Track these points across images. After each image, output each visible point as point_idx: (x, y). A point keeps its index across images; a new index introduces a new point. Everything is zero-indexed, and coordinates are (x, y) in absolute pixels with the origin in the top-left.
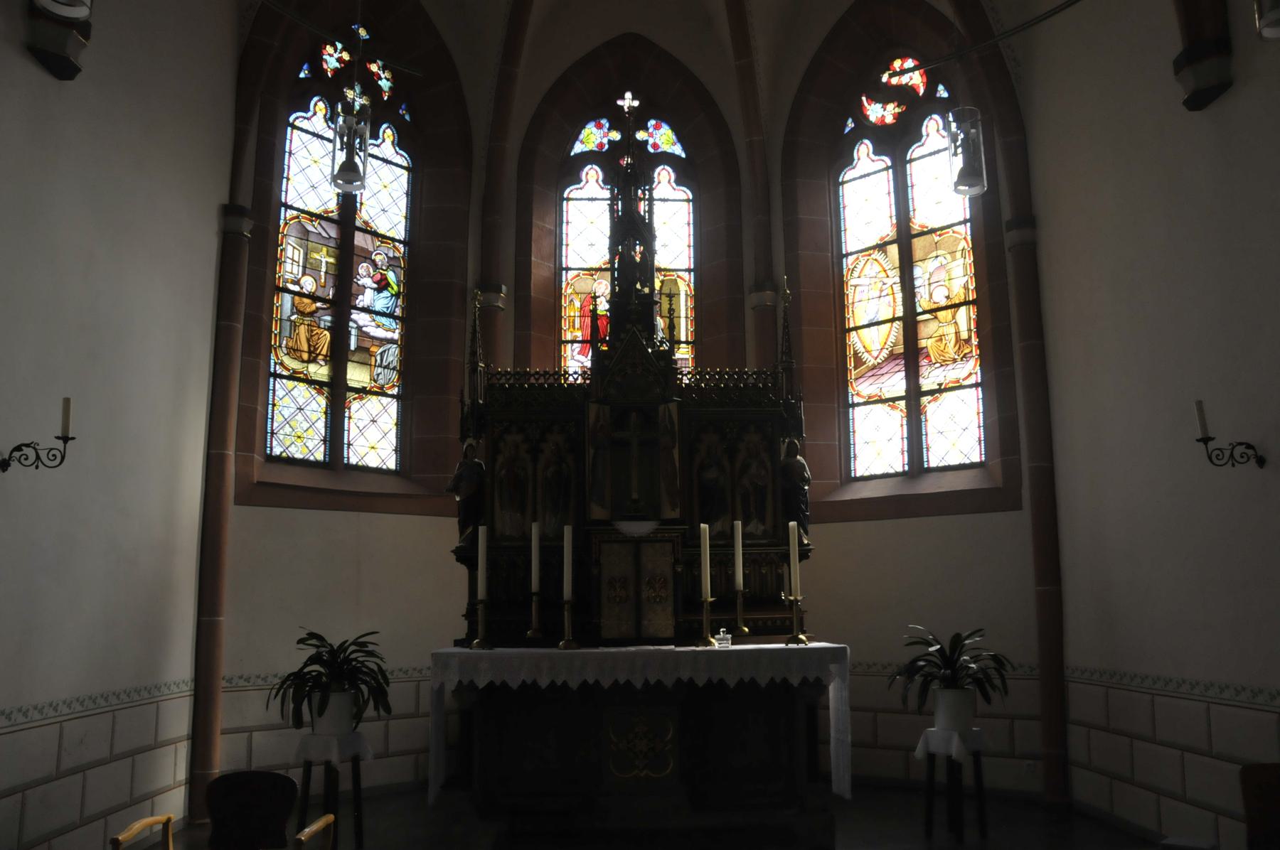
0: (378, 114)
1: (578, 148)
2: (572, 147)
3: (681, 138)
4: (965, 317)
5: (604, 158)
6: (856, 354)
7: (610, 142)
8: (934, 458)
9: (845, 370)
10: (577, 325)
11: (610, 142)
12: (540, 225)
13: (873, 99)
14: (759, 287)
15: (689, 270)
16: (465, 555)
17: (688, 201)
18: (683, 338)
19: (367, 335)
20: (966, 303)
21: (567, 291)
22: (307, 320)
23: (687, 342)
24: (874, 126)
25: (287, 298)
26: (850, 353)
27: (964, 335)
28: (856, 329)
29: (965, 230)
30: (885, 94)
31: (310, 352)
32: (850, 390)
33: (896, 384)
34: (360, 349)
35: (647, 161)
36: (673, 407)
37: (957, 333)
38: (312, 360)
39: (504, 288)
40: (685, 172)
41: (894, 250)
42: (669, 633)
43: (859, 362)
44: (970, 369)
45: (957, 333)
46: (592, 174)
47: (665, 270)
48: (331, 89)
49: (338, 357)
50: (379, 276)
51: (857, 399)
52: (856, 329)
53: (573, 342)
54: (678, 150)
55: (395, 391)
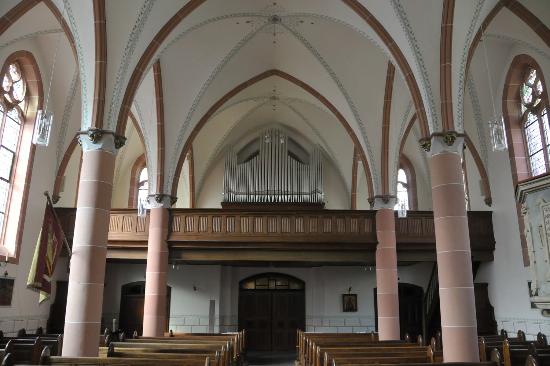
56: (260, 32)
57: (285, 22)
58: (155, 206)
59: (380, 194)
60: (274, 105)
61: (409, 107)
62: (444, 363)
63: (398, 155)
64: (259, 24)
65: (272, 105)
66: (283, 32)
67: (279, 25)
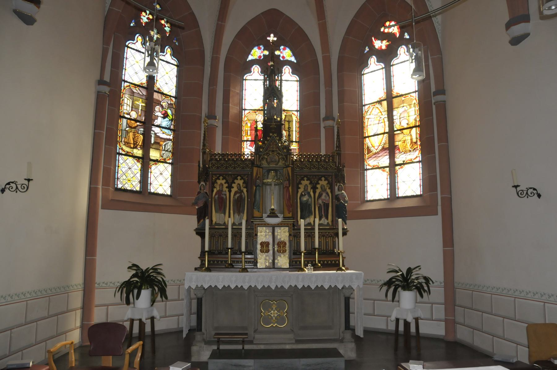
1: (250, 58)
4: (415, 133)
6: (368, 147)
7: (264, 55)
8: (401, 193)
9: (363, 154)
10: (249, 134)
11: (264, 55)
12: (234, 90)
13: (377, 39)
15: (297, 111)
17: (297, 81)
18: (294, 140)
19: (159, 137)
20: (415, 126)
22: (133, 130)
23: (296, 142)
26: (365, 147)
28: (368, 137)
29: (416, 95)
31: (134, 144)
32: (365, 163)
33: (385, 161)
34: (155, 143)
37: (411, 139)
38: (135, 147)
40: (296, 69)
41: (385, 103)
42: (287, 266)
43: (369, 151)
44: (416, 155)
45: (411, 139)
46: (256, 69)
47: (287, 111)
48: (144, 31)
50: (164, 112)
51: (368, 167)
52: (368, 137)
53: (247, 141)
54: (293, 59)
55: (170, 161)
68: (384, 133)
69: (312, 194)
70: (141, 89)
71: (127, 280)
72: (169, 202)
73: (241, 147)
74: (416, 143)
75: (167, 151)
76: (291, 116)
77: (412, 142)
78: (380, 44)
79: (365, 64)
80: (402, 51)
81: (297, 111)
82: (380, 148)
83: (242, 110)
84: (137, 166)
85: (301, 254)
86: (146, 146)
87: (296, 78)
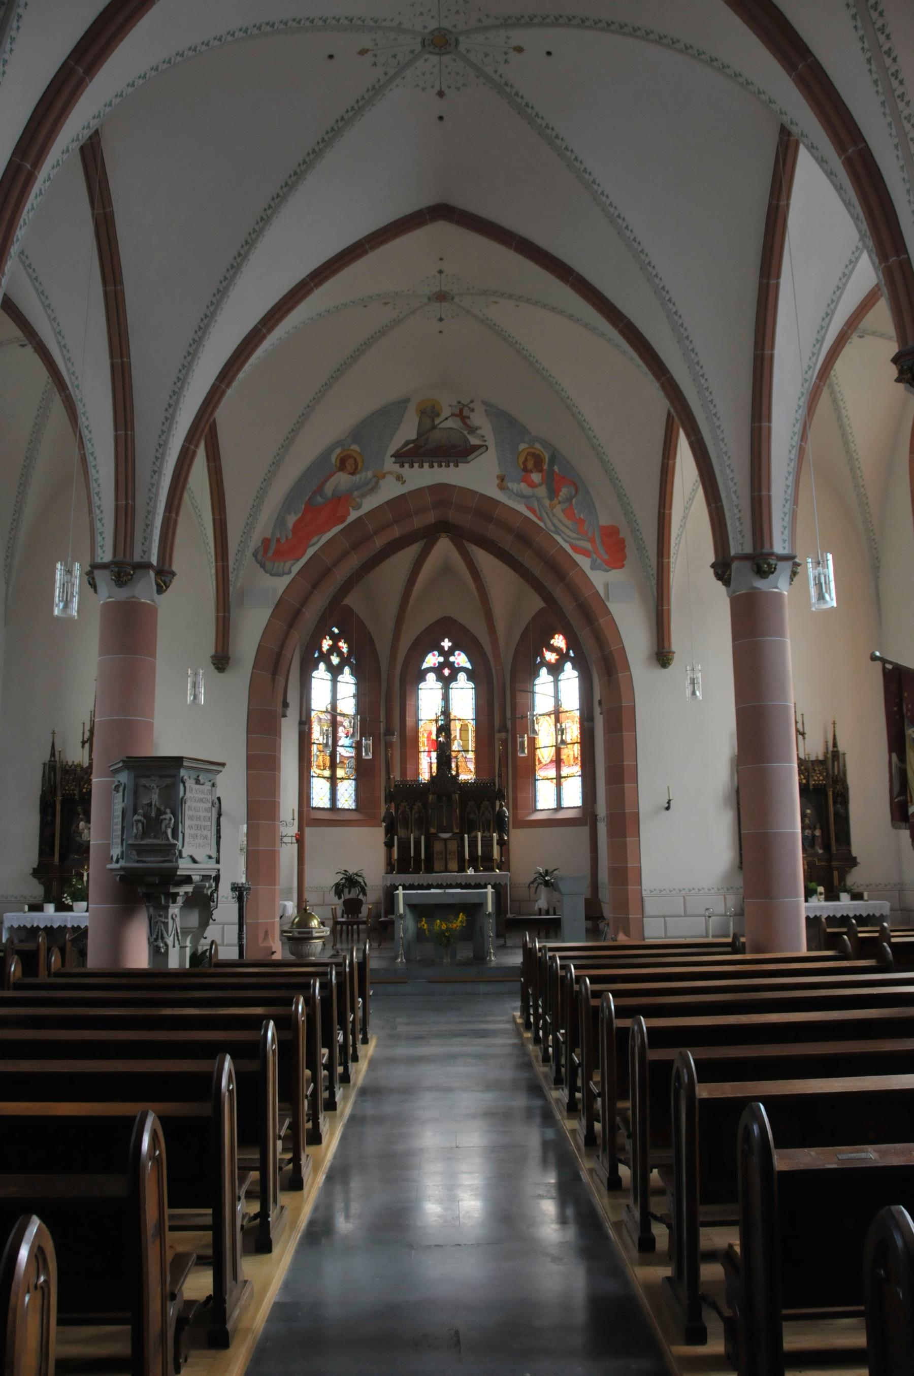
0: (344, 661)
1: (425, 666)
2: (422, 665)
3: (470, 660)
4: (577, 748)
5: (437, 670)
6: (539, 759)
7: (439, 663)
8: (565, 804)
9: (535, 765)
10: (426, 744)
11: (439, 663)
12: (409, 703)
13: (548, 650)
14: (500, 731)
15: (473, 719)
16: (389, 845)
17: (472, 688)
18: (470, 749)
19: (342, 756)
20: (577, 743)
21: (421, 730)
22: (322, 753)
23: (472, 751)
24: (547, 662)
25: (315, 746)
26: (537, 758)
27: (576, 756)
28: (539, 748)
29: (577, 713)
30: (553, 649)
31: (324, 766)
32: (537, 773)
33: (552, 773)
34: (341, 762)
35: (455, 671)
36: (457, 796)
37: (574, 755)
38: (325, 769)
39: (396, 733)
40: (472, 676)
41: (553, 716)
42: (457, 870)
43: (540, 762)
44: (577, 770)
45: (574, 755)
46: (431, 677)
47: (463, 720)
48: (325, 658)
49: (333, 766)
50: (346, 732)
51: (539, 778)
52: (539, 748)
53: (424, 752)
54: (469, 666)
55: (353, 777)
56: (397, 86)
57: (468, 51)
58: (110, 597)
59: (748, 549)
60: (443, 275)
61: (832, 303)
62: (179, 785)
63: (799, 443)
64: (395, 56)
65: (435, 317)
66: (464, 85)
67: (455, 60)
68: (552, 746)
69: (477, 812)
70: (326, 714)
71: (337, 882)
72: (355, 816)
73: (419, 758)
74: (577, 758)
75: (350, 768)
76: (467, 725)
77: (574, 757)
78: (551, 657)
79: (536, 675)
80: (568, 666)
81: (473, 719)
82: (549, 760)
83: (417, 720)
84: (326, 785)
85: (477, 861)
86: (333, 766)
87: (471, 685)
